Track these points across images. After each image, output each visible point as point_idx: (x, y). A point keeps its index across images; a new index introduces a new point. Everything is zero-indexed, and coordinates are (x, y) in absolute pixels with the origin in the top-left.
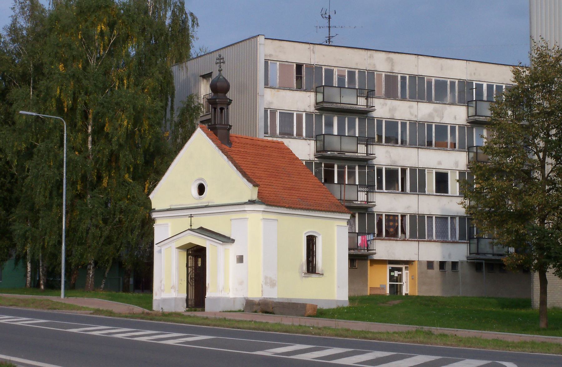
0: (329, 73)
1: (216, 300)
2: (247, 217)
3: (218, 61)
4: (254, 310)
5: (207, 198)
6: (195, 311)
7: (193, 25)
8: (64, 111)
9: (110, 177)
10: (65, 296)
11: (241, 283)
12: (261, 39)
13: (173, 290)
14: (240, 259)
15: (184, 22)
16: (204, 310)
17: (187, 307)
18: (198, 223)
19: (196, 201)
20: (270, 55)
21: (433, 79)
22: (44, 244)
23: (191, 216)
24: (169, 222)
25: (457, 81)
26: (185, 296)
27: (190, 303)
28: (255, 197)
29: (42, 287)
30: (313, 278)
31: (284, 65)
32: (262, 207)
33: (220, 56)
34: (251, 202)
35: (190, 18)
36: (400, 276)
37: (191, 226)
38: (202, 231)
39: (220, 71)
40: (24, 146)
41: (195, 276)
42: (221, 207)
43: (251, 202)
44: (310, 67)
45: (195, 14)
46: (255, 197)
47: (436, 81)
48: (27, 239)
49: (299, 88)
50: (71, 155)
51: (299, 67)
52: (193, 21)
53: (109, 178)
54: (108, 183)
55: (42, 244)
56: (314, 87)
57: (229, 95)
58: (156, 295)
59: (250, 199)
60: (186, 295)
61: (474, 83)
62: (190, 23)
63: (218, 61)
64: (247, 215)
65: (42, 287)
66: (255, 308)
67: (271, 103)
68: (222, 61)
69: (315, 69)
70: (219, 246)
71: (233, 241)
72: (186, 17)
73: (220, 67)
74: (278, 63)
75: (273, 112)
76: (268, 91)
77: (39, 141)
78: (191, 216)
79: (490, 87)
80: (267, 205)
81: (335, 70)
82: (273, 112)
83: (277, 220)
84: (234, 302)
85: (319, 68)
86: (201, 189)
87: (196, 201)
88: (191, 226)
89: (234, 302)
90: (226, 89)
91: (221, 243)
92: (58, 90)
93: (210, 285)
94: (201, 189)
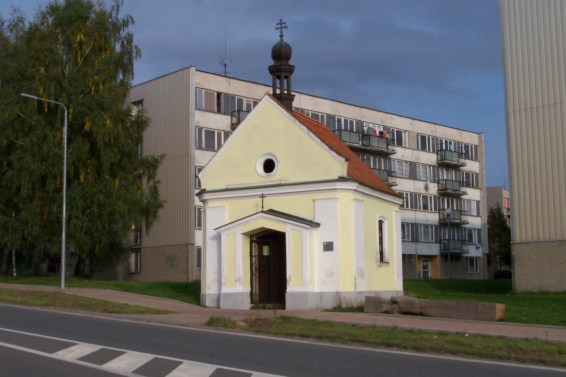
0: (240, 101)
1: (303, 296)
2: (337, 197)
3: (279, 26)
4: (384, 309)
5: (276, 176)
6: (264, 308)
7: (137, 56)
8: (44, 110)
9: (87, 173)
10: (65, 286)
11: (330, 275)
12: (193, 70)
13: (238, 284)
14: (328, 247)
15: (130, 53)
16: (284, 307)
17: (252, 303)
18: (272, 203)
19: (263, 180)
20: (199, 84)
21: (310, 112)
22: (24, 234)
23: (263, 196)
24: (227, 204)
25: (325, 115)
26: (248, 289)
27: (254, 298)
28: (345, 174)
29: (15, 274)
30: (384, 268)
31: (209, 93)
32: (353, 186)
33: (281, 21)
34: (341, 179)
35: (135, 50)
36: (427, 265)
37: (263, 207)
38: (271, 212)
39: (281, 36)
40: (5, 142)
41: (259, 266)
42: (290, 187)
43: (341, 179)
44: (227, 95)
45: (140, 47)
46: (345, 174)
47: (312, 114)
48: (7, 229)
49: (219, 111)
50: (56, 150)
51: (219, 94)
52: (137, 53)
53: (86, 174)
54: (84, 179)
55: (21, 234)
56: (230, 111)
57: (291, 62)
58: (209, 288)
59: (340, 175)
60: (250, 289)
61: (336, 117)
62: (134, 54)
63: (279, 26)
64: (337, 195)
65: (15, 274)
66: (386, 307)
67: (199, 122)
68: (283, 26)
69: (230, 98)
70: (303, 230)
71: (318, 225)
72: (131, 49)
73: (282, 33)
74: (204, 90)
75: (200, 130)
76: (197, 112)
77: (20, 138)
78: (263, 196)
79: (346, 121)
80: (361, 183)
81: (245, 99)
82: (200, 130)
83: (363, 201)
84: (321, 297)
85: (233, 97)
86: (269, 166)
87: (263, 180)
88: (263, 207)
89: (321, 297)
90: (288, 57)
91: (309, 227)
92: (42, 90)
93: (292, 277)
94: (269, 166)
